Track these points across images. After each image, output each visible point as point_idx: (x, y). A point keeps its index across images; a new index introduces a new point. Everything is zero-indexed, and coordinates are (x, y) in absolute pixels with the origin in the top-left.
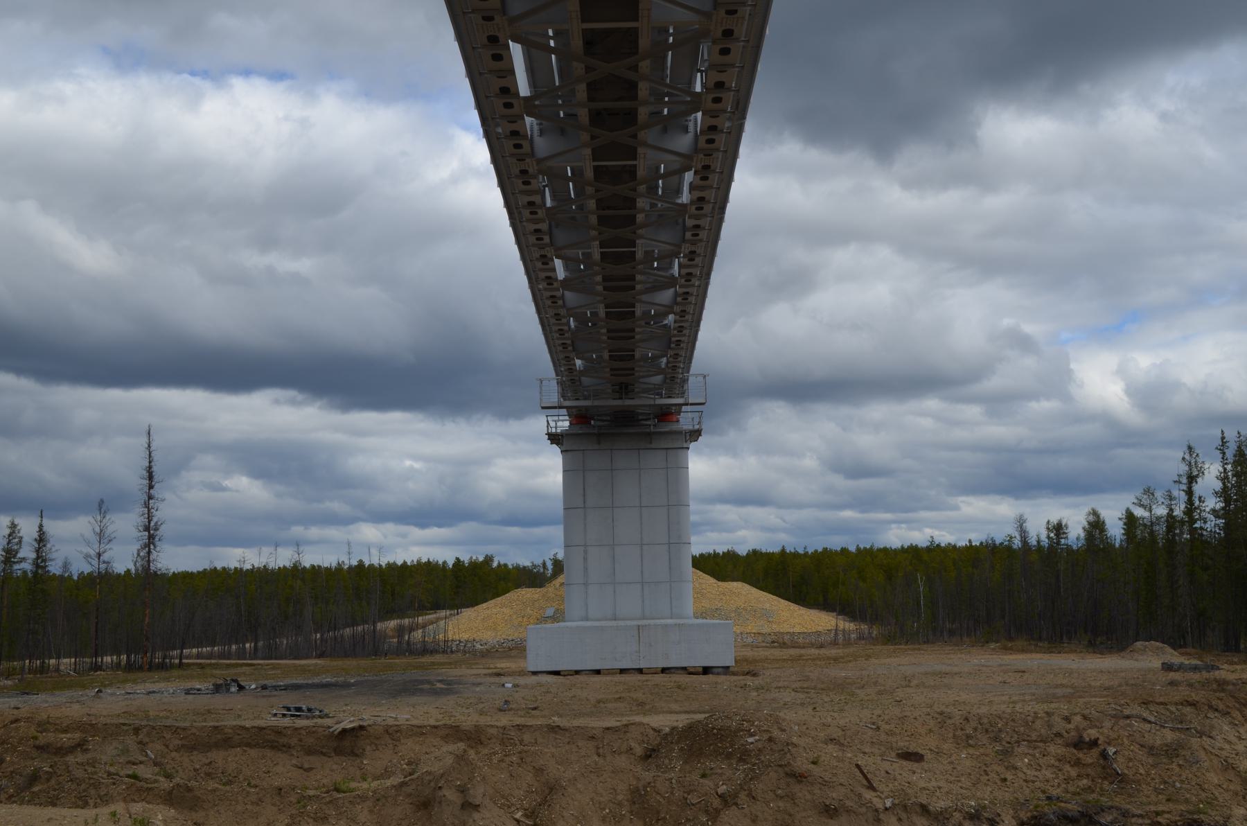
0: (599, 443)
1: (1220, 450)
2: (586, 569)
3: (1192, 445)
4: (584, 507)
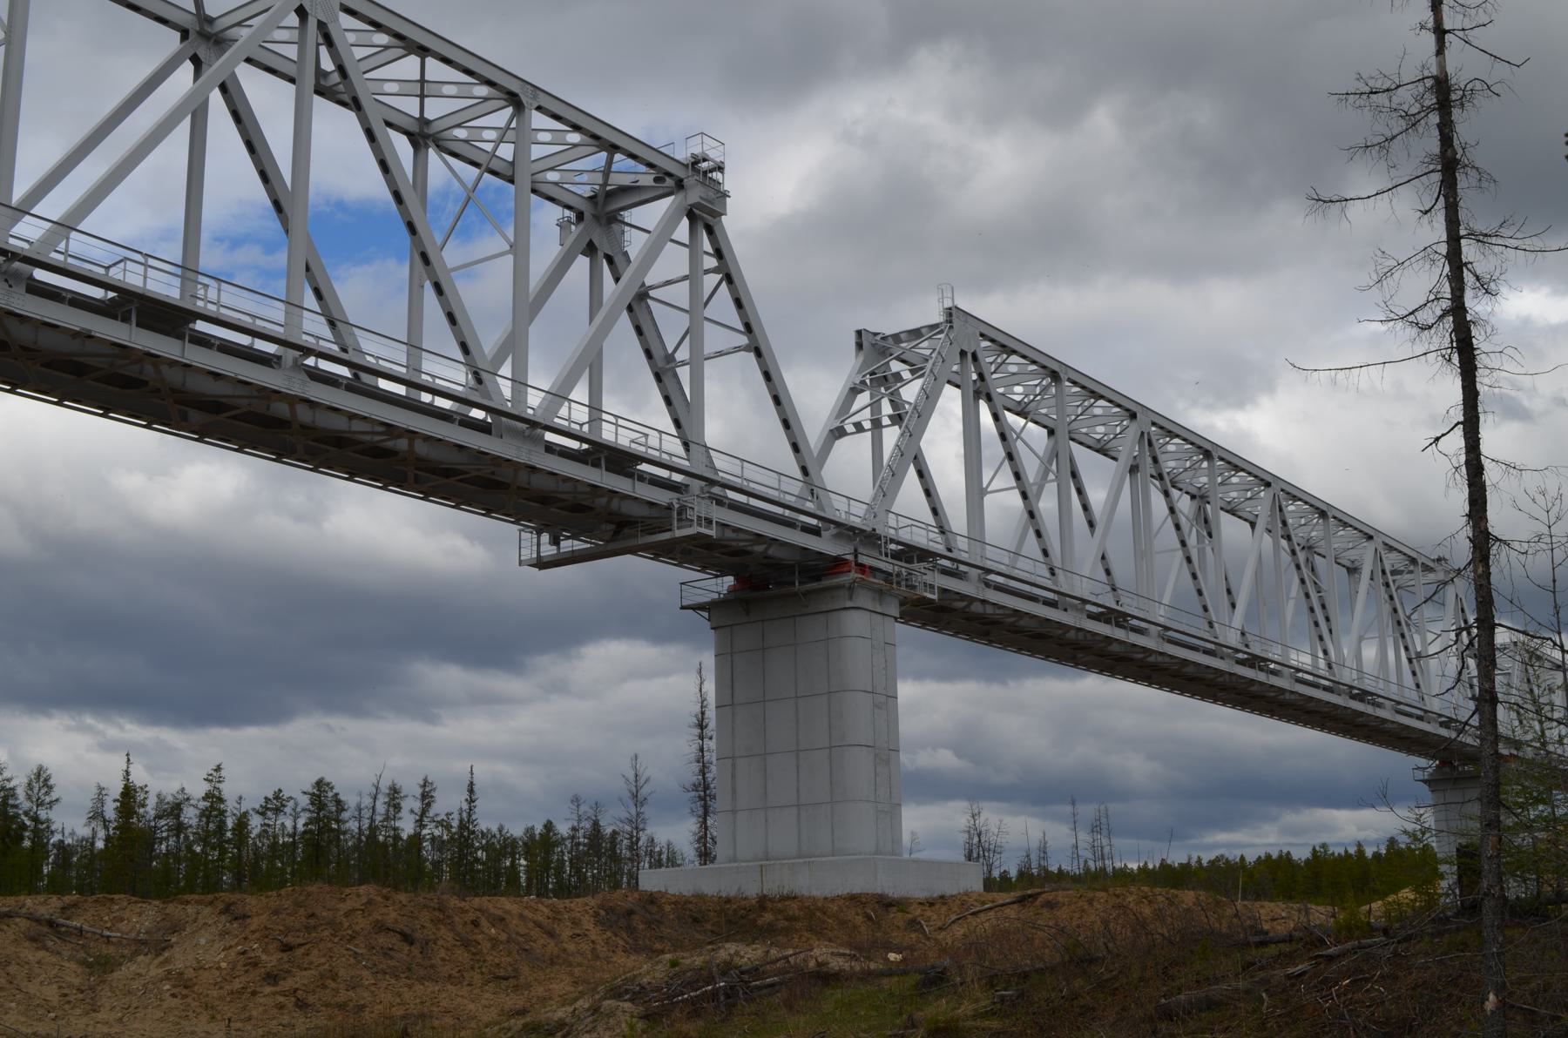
0: (748, 613)
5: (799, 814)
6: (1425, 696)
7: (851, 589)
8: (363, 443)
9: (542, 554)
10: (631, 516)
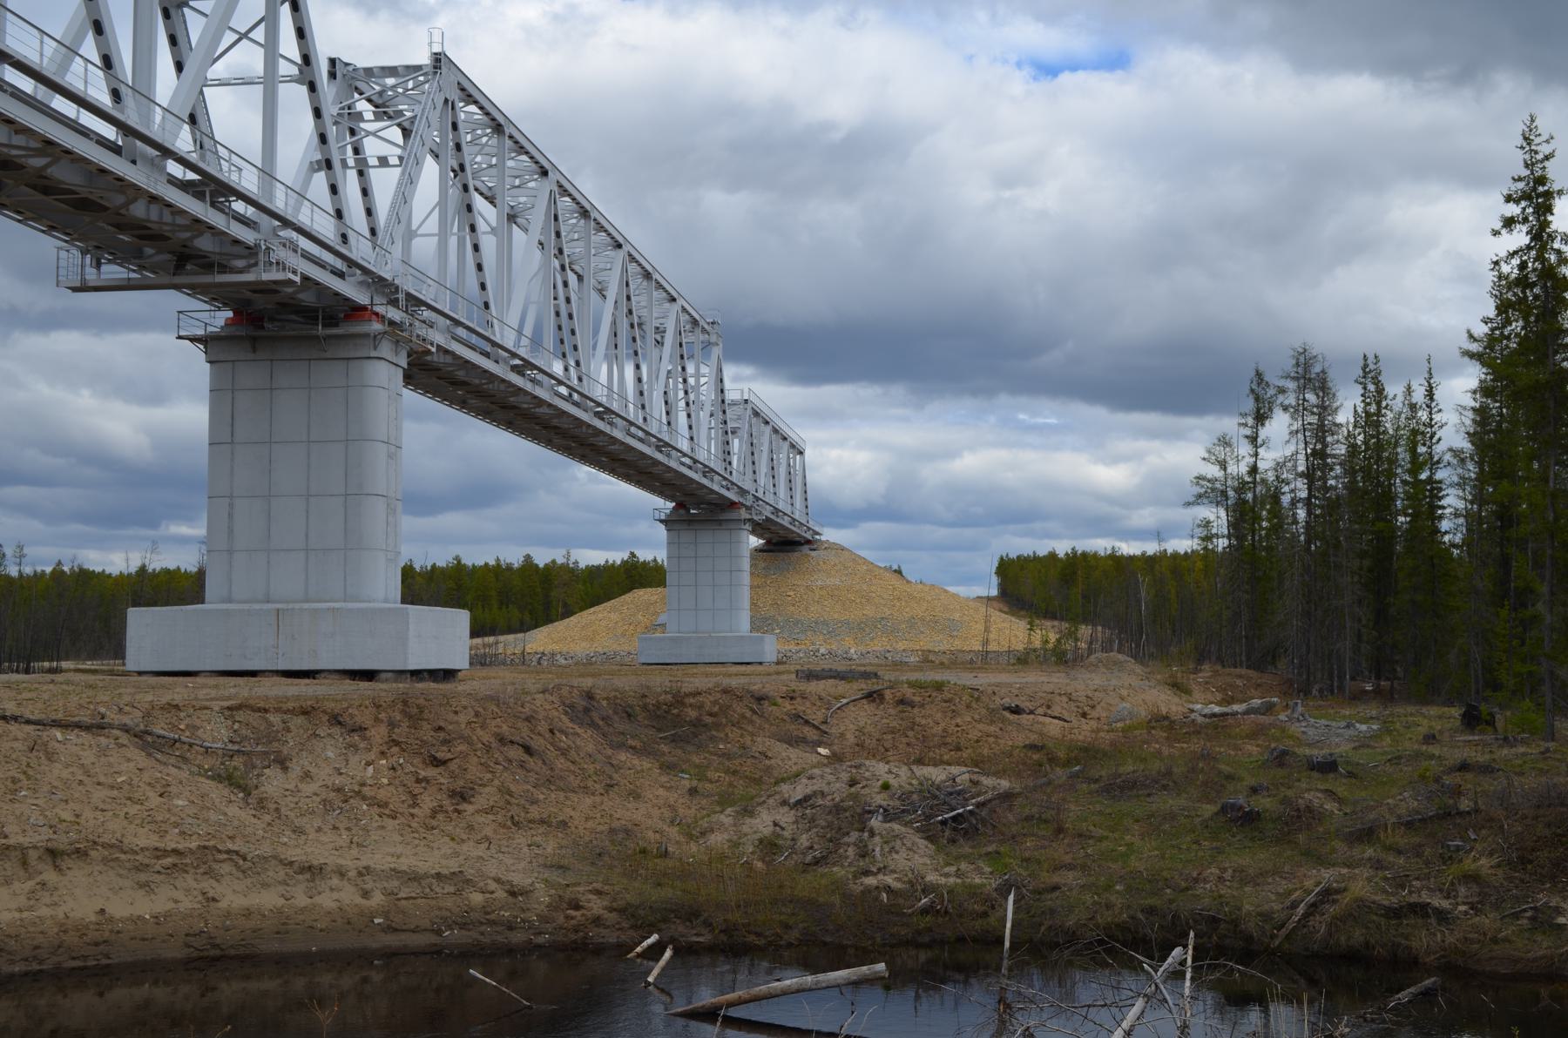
0: (254, 351)
1: (1361, 383)
2: (231, 531)
3: (1261, 369)
4: (232, 442)
5: (307, 559)
6: (495, 321)
7: (376, 339)
8: (205, 257)
9: (87, 277)
10: (201, 250)
